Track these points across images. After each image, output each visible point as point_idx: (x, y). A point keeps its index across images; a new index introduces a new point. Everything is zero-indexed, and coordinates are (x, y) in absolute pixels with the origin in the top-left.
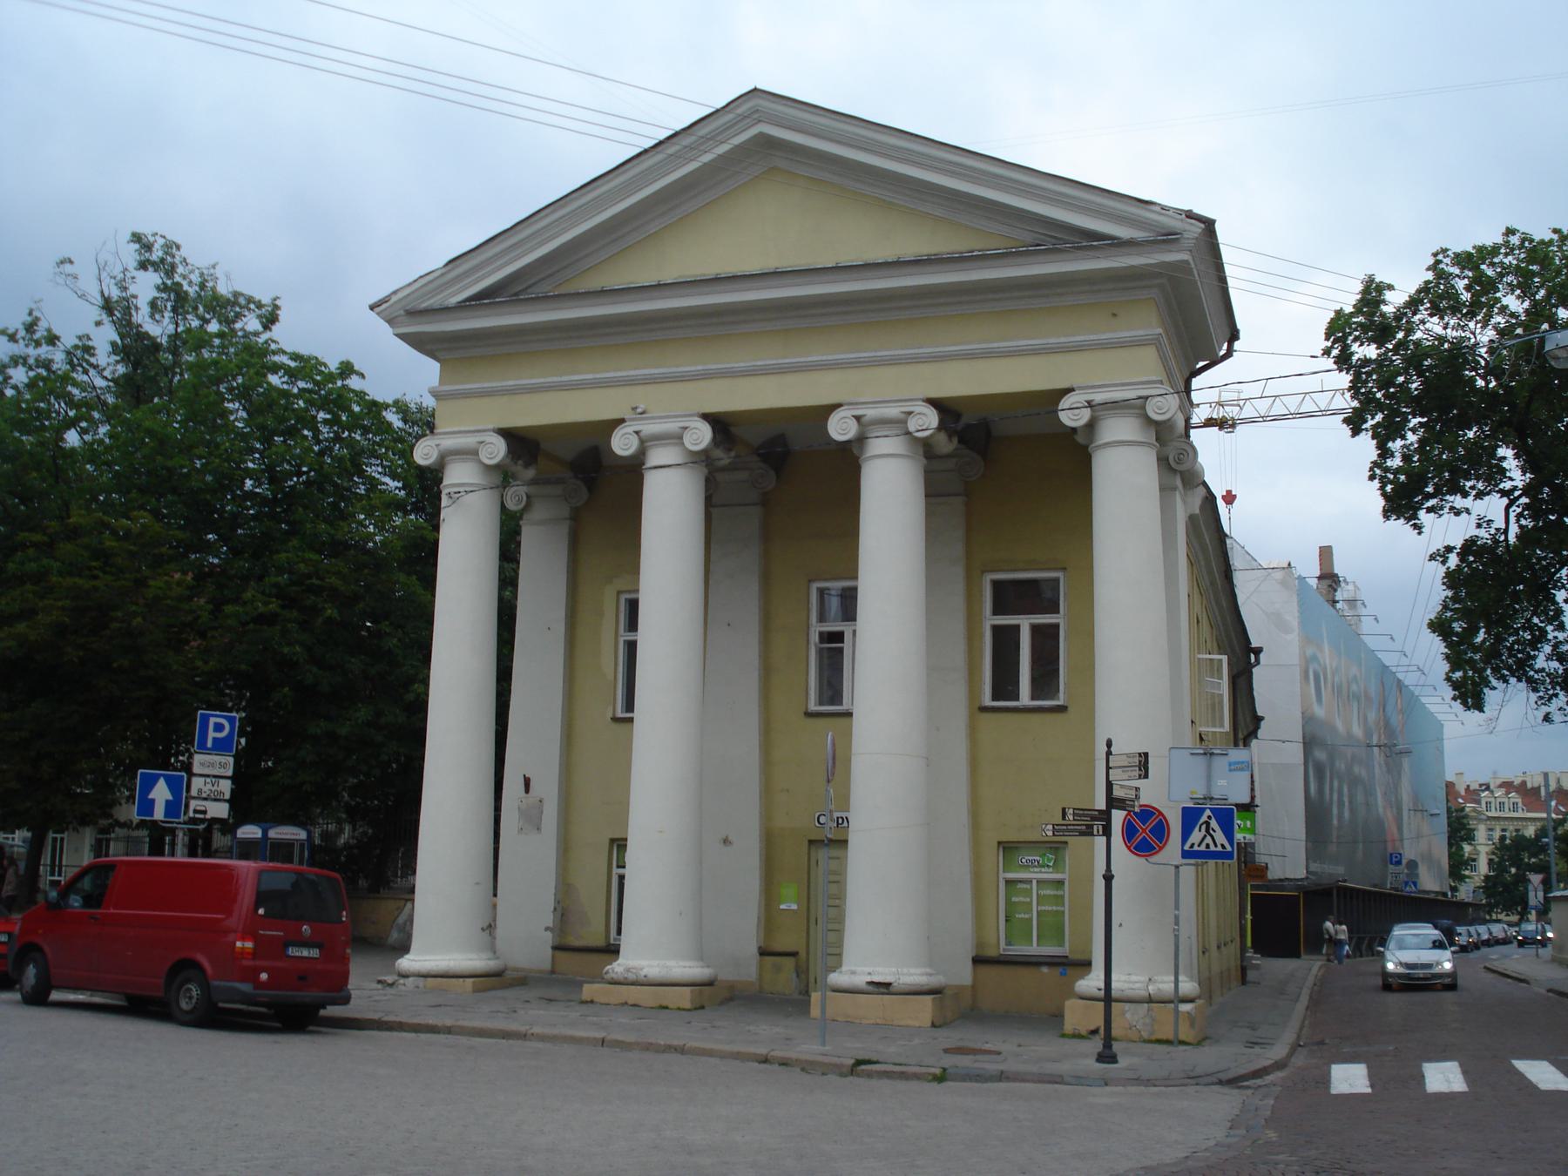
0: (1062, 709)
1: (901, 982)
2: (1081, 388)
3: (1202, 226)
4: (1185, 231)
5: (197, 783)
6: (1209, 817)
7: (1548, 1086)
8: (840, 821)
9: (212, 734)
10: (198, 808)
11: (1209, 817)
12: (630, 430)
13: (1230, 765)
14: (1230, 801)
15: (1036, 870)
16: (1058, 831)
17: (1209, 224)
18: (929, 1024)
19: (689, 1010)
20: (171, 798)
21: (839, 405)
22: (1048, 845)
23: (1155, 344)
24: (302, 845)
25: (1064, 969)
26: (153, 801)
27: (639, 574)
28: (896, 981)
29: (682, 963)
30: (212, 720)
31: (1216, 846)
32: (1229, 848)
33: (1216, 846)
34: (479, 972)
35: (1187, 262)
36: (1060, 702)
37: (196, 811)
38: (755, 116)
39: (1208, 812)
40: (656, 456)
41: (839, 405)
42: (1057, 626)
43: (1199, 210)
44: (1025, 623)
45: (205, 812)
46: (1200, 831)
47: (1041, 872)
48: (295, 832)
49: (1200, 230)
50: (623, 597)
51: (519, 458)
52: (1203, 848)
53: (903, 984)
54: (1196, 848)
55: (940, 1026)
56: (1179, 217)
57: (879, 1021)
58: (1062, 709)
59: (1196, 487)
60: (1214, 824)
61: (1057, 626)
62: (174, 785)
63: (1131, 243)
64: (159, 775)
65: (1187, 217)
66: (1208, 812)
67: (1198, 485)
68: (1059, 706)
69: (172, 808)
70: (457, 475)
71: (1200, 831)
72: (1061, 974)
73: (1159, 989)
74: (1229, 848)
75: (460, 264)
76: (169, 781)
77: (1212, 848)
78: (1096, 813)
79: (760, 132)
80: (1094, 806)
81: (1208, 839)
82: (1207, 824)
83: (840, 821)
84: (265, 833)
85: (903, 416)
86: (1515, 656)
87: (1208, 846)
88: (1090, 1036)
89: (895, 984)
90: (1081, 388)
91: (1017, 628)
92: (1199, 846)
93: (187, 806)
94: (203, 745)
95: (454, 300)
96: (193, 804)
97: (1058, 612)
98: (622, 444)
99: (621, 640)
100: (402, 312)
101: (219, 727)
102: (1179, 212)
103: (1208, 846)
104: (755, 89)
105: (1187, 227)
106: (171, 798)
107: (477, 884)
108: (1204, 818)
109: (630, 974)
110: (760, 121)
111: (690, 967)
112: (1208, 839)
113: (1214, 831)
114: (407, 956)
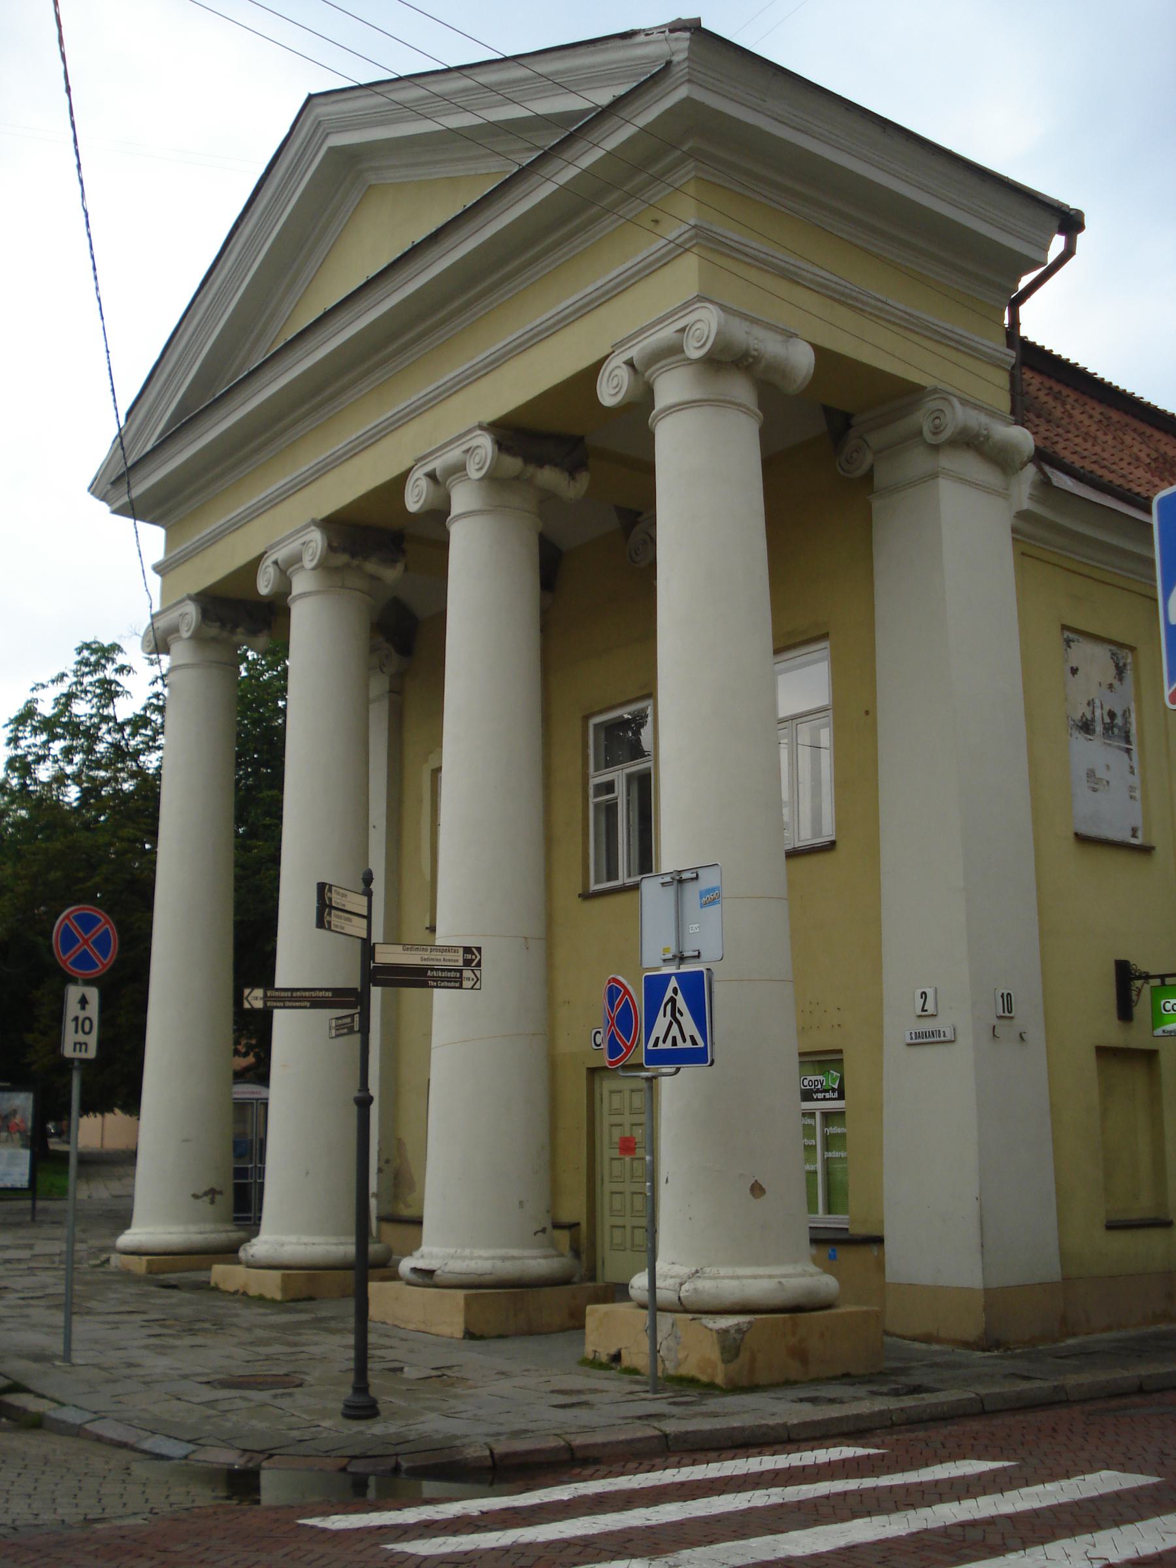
1: (447, 1269)
3: (687, 35)
4: (673, 54)
11: (675, 991)
15: (820, 1096)
17: (693, 27)
18: (458, 1332)
19: (281, 1302)
22: (814, 1058)
23: (697, 243)
25: (833, 1250)
27: (442, 747)
28: (439, 1268)
29: (305, 1239)
31: (684, 1040)
32: (701, 1044)
33: (684, 1040)
34: (174, 1248)
35: (688, 100)
38: (321, 130)
39: (673, 983)
43: (686, 16)
46: (665, 1016)
47: (824, 1099)
48: (254, 1090)
49: (686, 44)
51: (235, 626)
52: (668, 1045)
53: (450, 1272)
54: (661, 1046)
55: (481, 1337)
59: (1021, 469)
63: (618, 103)
65: (671, 31)
66: (673, 983)
67: (1024, 465)
71: (665, 1016)
72: (830, 1256)
73: (695, 1290)
74: (701, 1044)
75: (136, 415)
77: (680, 1044)
78: (330, 994)
80: (382, 990)
81: (675, 1031)
82: (673, 1001)
87: (674, 1042)
88: (613, 1365)
89: (438, 1272)
92: (664, 1041)
100: (109, 487)
102: (660, 29)
103: (674, 1042)
104: (311, 97)
107: (185, 1141)
108: (669, 993)
110: (328, 134)
111: (319, 1244)
113: (682, 1014)
114: (128, 1232)
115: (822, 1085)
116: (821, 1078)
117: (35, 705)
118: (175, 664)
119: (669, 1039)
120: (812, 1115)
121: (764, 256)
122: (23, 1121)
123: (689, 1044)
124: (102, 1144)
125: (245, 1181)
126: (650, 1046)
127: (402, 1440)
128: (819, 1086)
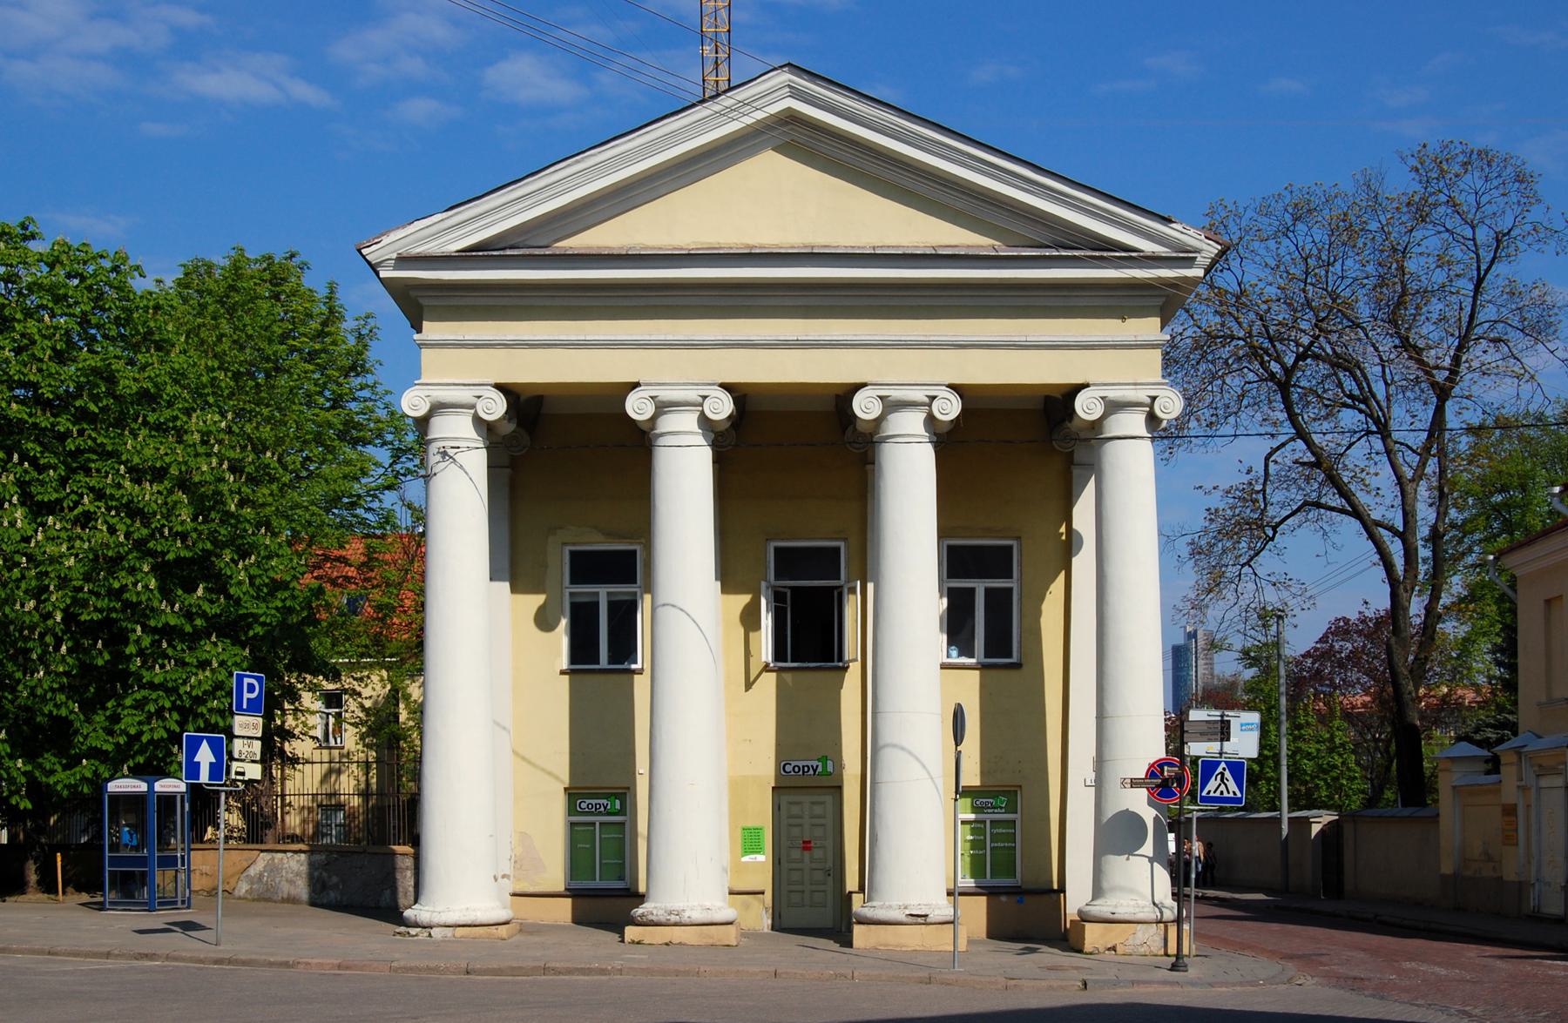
0: (1017, 666)
2: (1094, 385)
5: (238, 744)
6: (1224, 769)
7: (1178, 999)
8: (806, 769)
9: (246, 696)
10: (239, 770)
11: (1224, 769)
12: (646, 394)
13: (1242, 725)
14: (1240, 756)
15: (989, 811)
16: (1136, 784)
20: (214, 761)
21: (864, 385)
24: (182, 797)
26: (199, 763)
30: (246, 681)
32: (1239, 795)
36: (1014, 660)
37: (238, 773)
39: (1223, 765)
40: (668, 423)
41: (864, 385)
42: (1010, 590)
44: (980, 586)
45: (243, 774)
50: (567, 549)
52: (1218, 794)
54: (1212, 794)
56: (1198, 237)
57: (918, 948)
58: (1017, 666)
60: (1227, 774)
61: (1010, 590)
62: (216, 747)
64: (203, 737)
66: (1223, 765)
68: (1012, 663)
69: (215, 770)
70: (455, 429)
74: (1239, 795)
76: (210, 741)
77: (1226, 794)
79: (789, 108)
81: (1223, 788)
82: (1222, 774)
83: (806, 769)
84: (151, 787)
85: (927, 400)
86: (103, 348)
87: (1222, 793)
90: (1094, 385)
91: (972, 590)
93: (229, 768)
94: (240, 707)
95: (453, 248)
96: (235, 766)
97: (1011, 577)
98: (637, 407)
99: (567, 592)
101: (251, 688)
103: (1222, 793)
105: (1205, 247)
106: (214, 761)
107: (491, 836)
108: (1220, 770)
109: (673, 916)
112: (1223, 788)
115: (605, 808)
116: (605, 802)
117: (539, 600)
118: (507, 575)
119: (1218, 792)
120: (984, 822)
121: (512, 294)
122: (255, 727)
123: (1231, 795)
124: (257, 738)
125: (1195, 836)
126: (1204, 794)
127: (673, 918)
128: (602, 809)
